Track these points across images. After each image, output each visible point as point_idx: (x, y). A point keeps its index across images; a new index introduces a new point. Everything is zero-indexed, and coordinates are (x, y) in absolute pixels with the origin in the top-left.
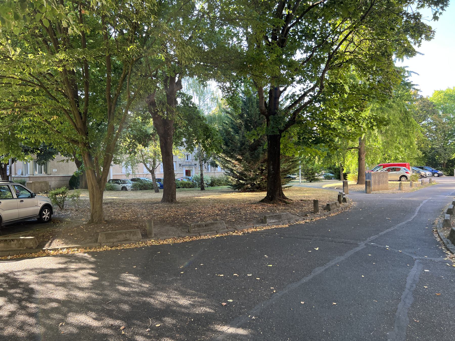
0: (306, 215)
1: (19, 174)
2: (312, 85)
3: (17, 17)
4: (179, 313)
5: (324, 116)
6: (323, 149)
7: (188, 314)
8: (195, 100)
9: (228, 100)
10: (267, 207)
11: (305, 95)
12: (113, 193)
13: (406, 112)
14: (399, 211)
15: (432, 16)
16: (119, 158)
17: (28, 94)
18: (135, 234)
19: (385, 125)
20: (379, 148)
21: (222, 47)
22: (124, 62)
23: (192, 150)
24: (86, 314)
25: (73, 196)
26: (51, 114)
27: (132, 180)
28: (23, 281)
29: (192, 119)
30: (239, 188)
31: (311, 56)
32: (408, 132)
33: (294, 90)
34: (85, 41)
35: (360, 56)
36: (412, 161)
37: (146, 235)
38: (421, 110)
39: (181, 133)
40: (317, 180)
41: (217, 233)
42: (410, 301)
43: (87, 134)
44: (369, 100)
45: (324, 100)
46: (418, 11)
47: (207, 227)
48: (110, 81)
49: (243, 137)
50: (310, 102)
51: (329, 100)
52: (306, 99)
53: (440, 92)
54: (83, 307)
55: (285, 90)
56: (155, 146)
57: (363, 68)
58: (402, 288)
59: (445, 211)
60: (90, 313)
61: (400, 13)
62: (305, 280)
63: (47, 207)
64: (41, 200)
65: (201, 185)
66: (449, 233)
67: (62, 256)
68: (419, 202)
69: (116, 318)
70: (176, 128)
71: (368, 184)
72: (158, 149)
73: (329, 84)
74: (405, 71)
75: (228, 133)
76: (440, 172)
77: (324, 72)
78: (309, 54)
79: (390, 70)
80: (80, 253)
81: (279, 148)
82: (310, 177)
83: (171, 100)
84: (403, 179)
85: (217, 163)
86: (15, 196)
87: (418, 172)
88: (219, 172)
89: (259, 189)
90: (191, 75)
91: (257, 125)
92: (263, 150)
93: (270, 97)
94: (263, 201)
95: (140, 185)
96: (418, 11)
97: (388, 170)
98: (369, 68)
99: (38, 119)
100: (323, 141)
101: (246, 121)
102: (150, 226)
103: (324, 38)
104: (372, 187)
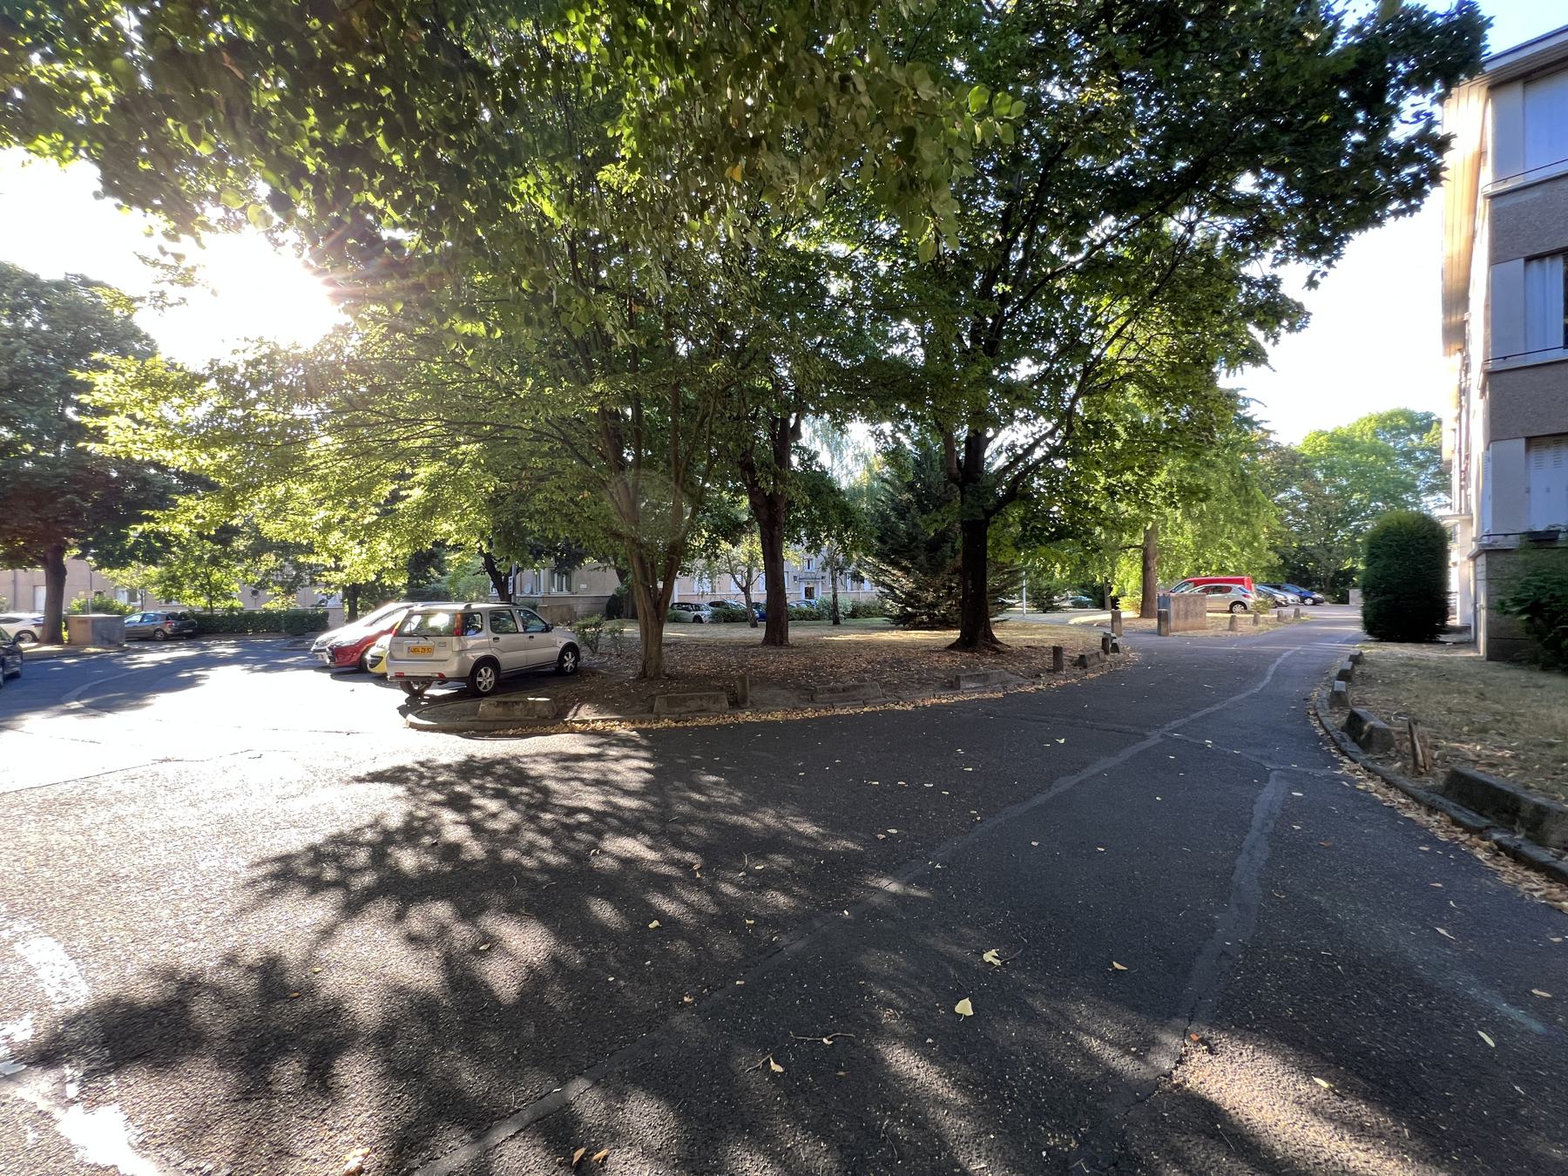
0: (1038, 676)
1: (527, 590)
2: (1050, 426)
3: (528, 322)
4: (797, 847)
5: (1076, 486)
6: (1069, 548)
7: (814, 852)
8: (825, 459)
9: (886, 455)
10: (962, 658)
11: (1037, 443)
12: (679, 626)
13: (1243, 475)
14: (1233, 671)
15: (1306, 280)
16: (687, 565)
17: (545, 455)
18: (717, 700)
19: (1202, 500)
20: (1186, 547)
21: (874, 361)
22: (702, 394)
23: (818, 551)
24: (635, 837)
25: (612, 631)
26: (580, 488)
27: (712, 604)
28: (532, 773)
29: (820, 493)
30: (905, 621)
31: (1048, 370)
32: (1248, 514)
33: (1013, 437)
34: (636, 361)
35: (1148, 367)
36: (1256, 573)
37: (737, 703)
38: (1277, 470)
39: (799, 521)
40: (1058, 609)
41: (865, 705)
42: (1262, 854)
43: (637, 523)
44: (1166, 453)
45: (1074, 455)
46: (1275, 271)
47: (847, 694)
48: (677, 428)
49: (915, 525)
50: (1046, 459)
51: (1085, 454)
52: (1039, 453)
53: (1320, 434)
54: (630, 826)
55: (995, 436)
56: (751, 544)
57: (1154, 390)
58: (1245, 827)
59: (1334, 674)
60: (640, 836)
61: (1235, 279)
62: (1039, 800)
63: (570, 647)
64: (561, 637)
65: (833, 615)
66: (1344, 719)
67: (595, 733)
68: (1273, 657)
69: (686, 848)
70: (790, 512)
71: (1163, 618)
72: (758, 548)
73: (1085, 424)
74: (1236, 397)
75: (885, 518)
76: (1317, 596)
77: (1074, 400)
78: (1043, 367)
79: (1212, 393)
80: (622, 730)
81: (985, 547)
82: (1044, 601)
83: (782, 456)
84: (1238, 608)
85: (864, 574)
86: (521, 629)
87: (1270, 595)
88: (868, 592)
89: (944, 624)
90: (817, 414)
91: (941, 503)
92: (953, 550)
93: (967, 450)
94: (953, 647)
95: (725, 614)
96: (1275, 271)
97: (1206, 591)
98: (1166, 390)
99: (559, 497)
100: (1070, 534)
101: (918, 496)
102: (744, 687)
103: (1074, 333)
104: (1172, 624)
